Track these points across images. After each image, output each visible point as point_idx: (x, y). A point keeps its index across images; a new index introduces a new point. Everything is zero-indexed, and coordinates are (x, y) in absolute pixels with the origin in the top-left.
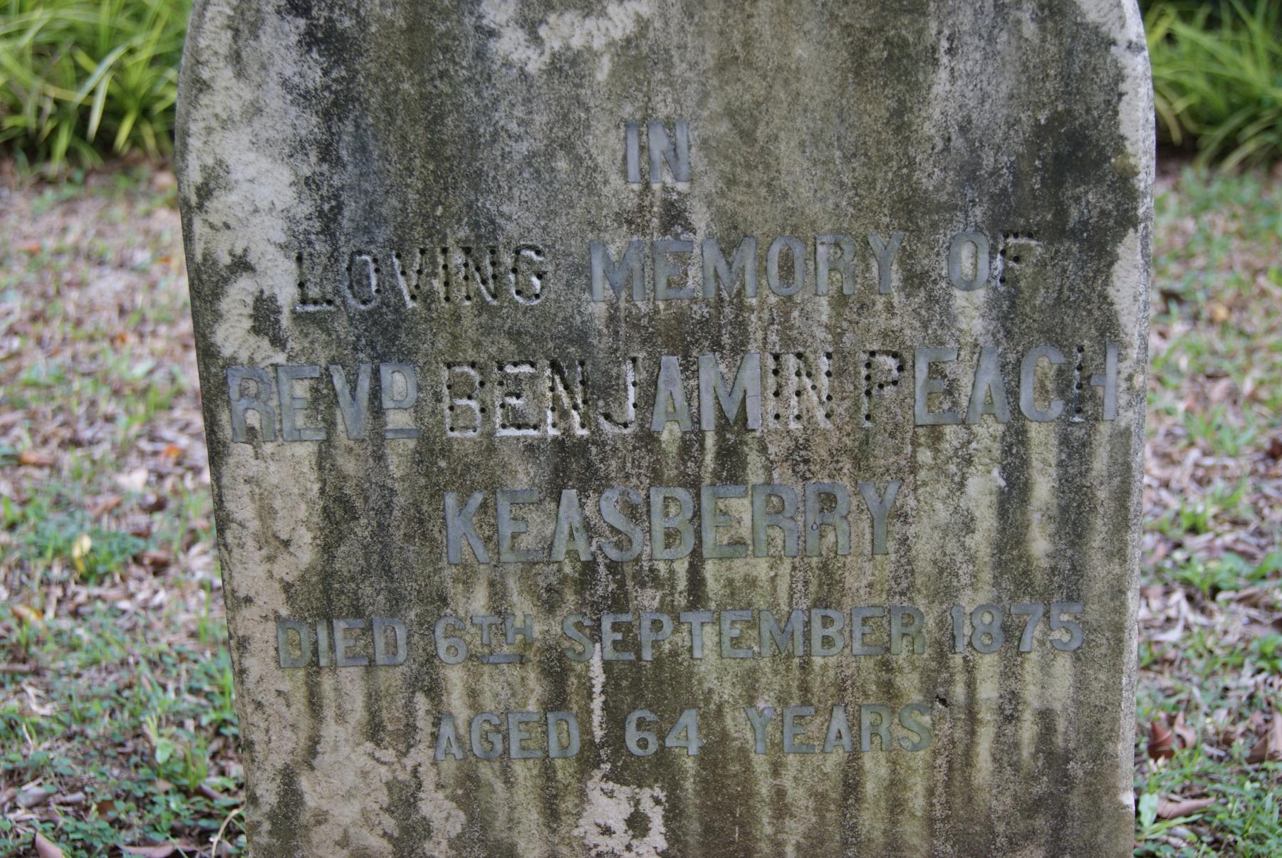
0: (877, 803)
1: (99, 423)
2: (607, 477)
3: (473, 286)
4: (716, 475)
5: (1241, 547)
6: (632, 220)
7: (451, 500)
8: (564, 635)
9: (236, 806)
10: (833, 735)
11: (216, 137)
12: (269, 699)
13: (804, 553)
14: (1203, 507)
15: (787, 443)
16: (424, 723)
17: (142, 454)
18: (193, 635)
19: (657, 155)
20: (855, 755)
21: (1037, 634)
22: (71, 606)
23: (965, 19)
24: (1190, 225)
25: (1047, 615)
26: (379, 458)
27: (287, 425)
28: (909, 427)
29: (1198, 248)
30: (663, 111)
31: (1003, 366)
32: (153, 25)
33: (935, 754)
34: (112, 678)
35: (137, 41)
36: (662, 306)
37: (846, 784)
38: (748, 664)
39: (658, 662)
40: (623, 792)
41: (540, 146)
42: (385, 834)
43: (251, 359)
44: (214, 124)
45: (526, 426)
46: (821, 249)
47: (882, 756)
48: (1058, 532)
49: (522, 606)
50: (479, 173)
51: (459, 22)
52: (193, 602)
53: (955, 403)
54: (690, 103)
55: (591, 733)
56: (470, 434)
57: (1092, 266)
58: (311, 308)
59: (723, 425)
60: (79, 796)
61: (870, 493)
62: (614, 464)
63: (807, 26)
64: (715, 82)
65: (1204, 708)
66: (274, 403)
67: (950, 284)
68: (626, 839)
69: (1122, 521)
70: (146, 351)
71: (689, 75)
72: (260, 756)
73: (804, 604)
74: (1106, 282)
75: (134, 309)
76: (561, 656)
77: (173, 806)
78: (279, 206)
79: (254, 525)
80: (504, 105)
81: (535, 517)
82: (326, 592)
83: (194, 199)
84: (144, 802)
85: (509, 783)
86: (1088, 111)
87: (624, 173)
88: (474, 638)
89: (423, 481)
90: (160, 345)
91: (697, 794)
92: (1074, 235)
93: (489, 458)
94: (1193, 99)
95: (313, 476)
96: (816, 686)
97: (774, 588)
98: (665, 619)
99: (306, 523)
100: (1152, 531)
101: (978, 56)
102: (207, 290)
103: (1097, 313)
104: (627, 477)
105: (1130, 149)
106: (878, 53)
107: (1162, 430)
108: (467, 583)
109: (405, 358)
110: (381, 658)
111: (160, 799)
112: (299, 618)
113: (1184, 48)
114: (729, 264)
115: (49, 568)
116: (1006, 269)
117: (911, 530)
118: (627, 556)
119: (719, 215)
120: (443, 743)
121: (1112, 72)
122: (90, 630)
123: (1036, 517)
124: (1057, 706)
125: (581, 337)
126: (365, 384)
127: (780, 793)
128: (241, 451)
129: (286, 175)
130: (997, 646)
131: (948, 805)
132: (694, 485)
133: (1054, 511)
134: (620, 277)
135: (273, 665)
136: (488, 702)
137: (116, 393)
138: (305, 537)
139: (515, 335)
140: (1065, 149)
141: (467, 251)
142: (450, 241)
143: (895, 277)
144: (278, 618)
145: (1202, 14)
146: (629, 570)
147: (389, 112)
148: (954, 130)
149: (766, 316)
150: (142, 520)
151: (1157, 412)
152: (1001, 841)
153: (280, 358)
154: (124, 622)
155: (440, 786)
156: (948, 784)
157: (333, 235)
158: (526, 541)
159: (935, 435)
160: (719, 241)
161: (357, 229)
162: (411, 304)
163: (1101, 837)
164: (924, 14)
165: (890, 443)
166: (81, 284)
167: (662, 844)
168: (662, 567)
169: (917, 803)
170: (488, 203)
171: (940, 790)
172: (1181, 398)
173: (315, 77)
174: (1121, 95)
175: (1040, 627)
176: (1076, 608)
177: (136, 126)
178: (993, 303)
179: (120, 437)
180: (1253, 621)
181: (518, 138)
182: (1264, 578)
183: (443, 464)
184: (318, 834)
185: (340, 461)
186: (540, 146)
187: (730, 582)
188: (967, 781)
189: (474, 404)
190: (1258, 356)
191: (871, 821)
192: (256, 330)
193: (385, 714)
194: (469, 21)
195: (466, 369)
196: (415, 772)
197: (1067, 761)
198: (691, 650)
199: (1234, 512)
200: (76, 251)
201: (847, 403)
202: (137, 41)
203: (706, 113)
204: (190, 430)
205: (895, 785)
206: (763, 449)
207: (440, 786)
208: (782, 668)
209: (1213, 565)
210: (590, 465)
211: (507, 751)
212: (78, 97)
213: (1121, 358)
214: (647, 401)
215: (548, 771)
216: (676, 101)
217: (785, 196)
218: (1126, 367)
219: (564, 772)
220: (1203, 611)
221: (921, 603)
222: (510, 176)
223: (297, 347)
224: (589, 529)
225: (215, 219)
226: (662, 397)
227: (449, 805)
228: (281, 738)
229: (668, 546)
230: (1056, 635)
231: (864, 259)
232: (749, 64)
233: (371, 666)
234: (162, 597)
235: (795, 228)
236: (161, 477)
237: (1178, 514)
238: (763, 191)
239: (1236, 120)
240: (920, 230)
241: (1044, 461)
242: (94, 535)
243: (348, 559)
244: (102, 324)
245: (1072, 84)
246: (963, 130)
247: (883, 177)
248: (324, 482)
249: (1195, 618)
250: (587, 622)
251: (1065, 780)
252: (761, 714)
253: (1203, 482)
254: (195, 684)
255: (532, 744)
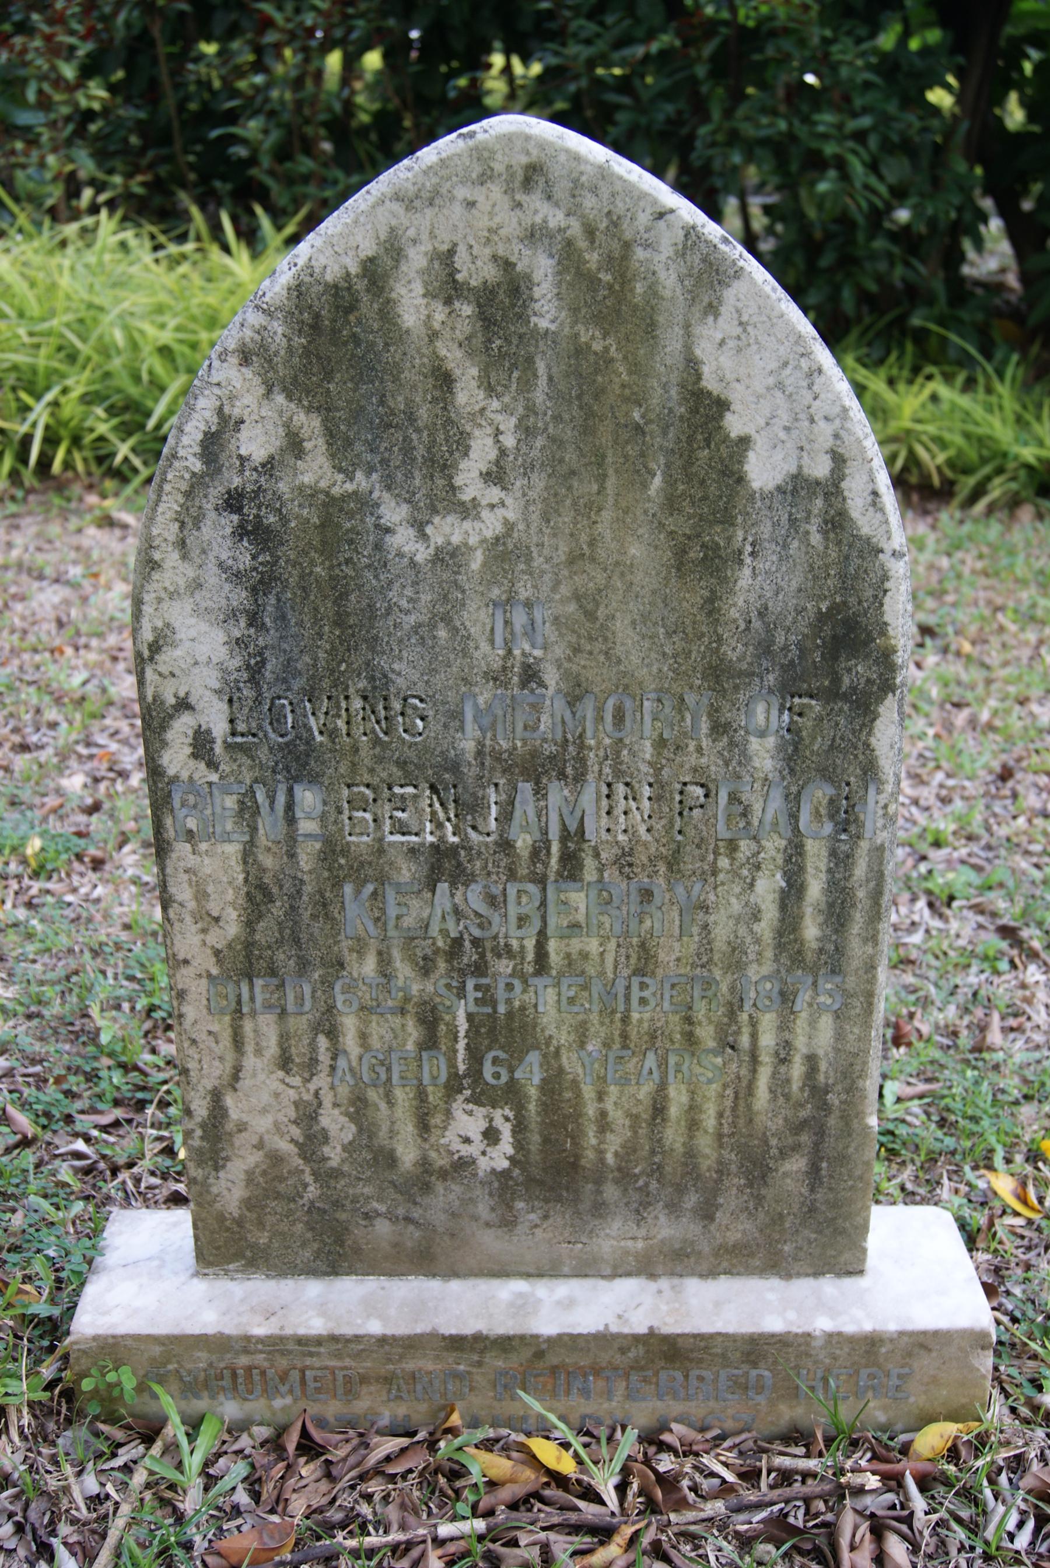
0: (678, 1122)
1: (44, 730)
2: (472, 874)
3: (369, 725)
4: (559, 874)
5: (974, 860)
6: (497, 678)
7: (348, 889)
8: (437, 993)
9: (165, 1082)
10: (645, 1071)
11: (165, 605)
12: (201, 1036)
13: (627, 934)
14: (946, 826)
15: (616, 850)
16: (324, 1057)
17: (80, 756)
18: (127, 927)
19: (518, 628)
20: (662, 1086)
21: (807, 998)
22: (26, 899)
23: (766, 530)
24: (945, 562)
25: (815, 984)
26: (292, 855)
27: (218, 829)
28: (712, 841)
29: (949, 585)
30: (524, 594)
31: (787, 796)
32: (84, 367)
33: (725, 1086)
34: (61, 964)
35: (69, 382)
36: (519, 744)
37: (655, 1108)
38: (580, 1017)
39: (510, 1015)
40: (480, 1111)
41: (425, 618)
42: (292, 1140)
43: (191, 777)
44: (163, 595)
45: (410, 833)
46: (646, 703)
47: (683, 1088)
48: (826, 922)
49: (403, 970)
50: (376, 638)
51: (362, 521)
52: (125, 897)
53: (748, 823)
54: (545, 589)
55: (456, 1067)
56: (365, 838)
57: (858, 721)
58: (239, 739)
59: (565, 836)
60: (38, 1069)
61: (680, 890)
62: (478, 864)
63: (640, 531)
64: (566, 572)
65: (938, 1004)
66: (208, 812)
67: (747, 732)
68: (482, 1147)
69: (876, 915)
70: (80, 662)
71: (545, 566)
72: (194, 1080)
73: (626, 972)
74: (870, 734)
75: (69, 622)
76: (434, 1009)
77: (115, 1081)
78: (215, 660)
79: (192, 905)
80: (396, 586)
81: (415, 903)
82: (248, 956)
83: (146, 653)
84: (92, 1077)
85: (391, 1103)
86: (860, 603)
87: (492, 642)
88: (365, 995)
89: (326, 874)
90: (92, 657)
91: (538, 1114)
92: (845, 697)
93: (379, 857)
94: (952, 452)
95: (239, 868)
96: (633, 1034)
97: (603, 961)
98: (516, 982)
99: (233, 904)
100: (902, 845)
101: (775, 558)
102: (155, 724)
103: (861, 757)
104: (489, 874)
105: (891, 632)
106: (695, 553)
107: (915, 753)
108: (360, 952)
109: (314, 779)
110: (291, 1008)
111: (104, 1073)
112: (226, 976)
113: (945, 407)
114: (574, 714)
115: (7, 864)
116: (792, 722)
117: (712, 918)
118: (487, 934)
119: (566, 675)
120: (339, 1073)
121: (880, 573)
122: (42, 921)
123: (808, 911)
124: (821, 1052)
125: (455, 767)
126: (281, 799)
127: (603, 1114)
128: (182, 849)
129: (221, 637)
130: (775, 1006)
131: (734, 1124)
132: (541, 881)
133: (823, 906)
134: (486, 721)
135: (205, 1011)
136: (375, 1043)
137: (58, 701)
138: (232, 915)
139: (402, 764)
140: (840, 631)
141: (365, 698)
142: (351, 690)
143: (705, 726)
144: (209, 976)
145: (961, 378)
146: (488, 945)
147: (304, 589)
148: (754, 615)
149: (601, 753)
150: (82, 818)
151: (911, 737)
152: (774, 1151)
153: (214, 777)
154: (69, 913)
155: (336, 1105)
156: (734, 1109)
157: (257, 684)
158: (408, 922)
159: (732, 846)
160: (566, 695)
161: (277, 679)
162: (319, 738)
163: (851, 1150)
164: (733, 525)
165: (697, 852)
166: (22, 598)
167: (510, 1151)
168: (515, 944)
169: (710, 1122)
170: (383, 662)
171: (728, 1113)
172: (931, 725)
173: (245, 561)
174: (886, 591)
175: (810, 993)
176: (838, 979)
177: (69, 452)
178: (781, 748)
179: (61, 742)
180: (980, 926)
181: (408, 612)
182: (990, 888)
183: (342, 861)
184: (239, 1140)
185: (261, 857)
186: (425, 618)
187: (568, 955)
188: (749, 1107)
189: (368, 816)
190: (994, 687)
191: (673, 1136)
192: (195, 756)
193: (293, 1050)
194: (370, 521)
195: (363, 789)
196: (317, 1094)
197: (827, 1093)
198: (536, 1006)
199: (969, 829)
200: (20, 566)
201: (663, 822)
202: (69, 382)
203: (557, 597)
204: (119, 737)
205: (693, 1109)
206: (597, 855)
207: (336, 1105)
208: (607, 1021)
209: (951, 876)
210: (459, 864)
211: (389, 1079)
212: (24, 429)
213: (879, 792)
214: (506, 816)
215: (421, 1095)
216: (535, 587)
217: (619, 662)
218: (883, 799)
219: (434, 1096)
220: (941, 916)
221: (717, 973)
222: (400, 641)
223: (228, 769)
224: (457, 912)
225: (163, 669)
226: (518, 813)
227: (344, 1119)
228: (211, 1066)
229: (520, 927)
230: (822, 999)
231: (680, 712)
232: (593, 560)
233: (283, 1013)
234: (99, 891)
235: (626, 687)
236: (97, 780)
237: (925, 830)
238: (602, 658)
239: (987, 470)
240: (724, 690)
241: (817, 868)
242: (42, 835)
243: (266, 931)
244: (44, 638)
245: (848, 582)
246: (761, 615)
247: (697, 649)
248: (248, 873)
249: (936, 923)
250: (455, 984)
251: (825, 1107)
252: (590, 1054)
253: (945, 801)
254: (129, 972)
255: (409, 1075)
